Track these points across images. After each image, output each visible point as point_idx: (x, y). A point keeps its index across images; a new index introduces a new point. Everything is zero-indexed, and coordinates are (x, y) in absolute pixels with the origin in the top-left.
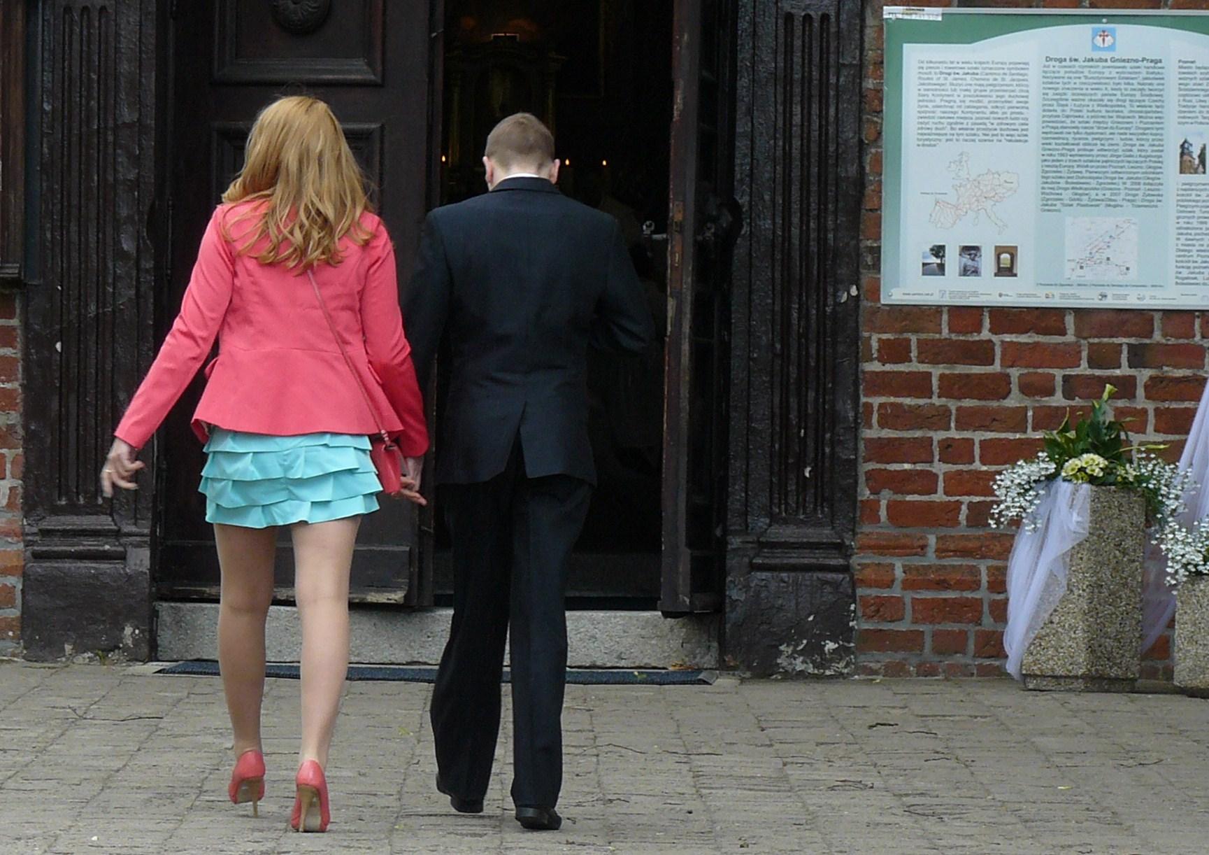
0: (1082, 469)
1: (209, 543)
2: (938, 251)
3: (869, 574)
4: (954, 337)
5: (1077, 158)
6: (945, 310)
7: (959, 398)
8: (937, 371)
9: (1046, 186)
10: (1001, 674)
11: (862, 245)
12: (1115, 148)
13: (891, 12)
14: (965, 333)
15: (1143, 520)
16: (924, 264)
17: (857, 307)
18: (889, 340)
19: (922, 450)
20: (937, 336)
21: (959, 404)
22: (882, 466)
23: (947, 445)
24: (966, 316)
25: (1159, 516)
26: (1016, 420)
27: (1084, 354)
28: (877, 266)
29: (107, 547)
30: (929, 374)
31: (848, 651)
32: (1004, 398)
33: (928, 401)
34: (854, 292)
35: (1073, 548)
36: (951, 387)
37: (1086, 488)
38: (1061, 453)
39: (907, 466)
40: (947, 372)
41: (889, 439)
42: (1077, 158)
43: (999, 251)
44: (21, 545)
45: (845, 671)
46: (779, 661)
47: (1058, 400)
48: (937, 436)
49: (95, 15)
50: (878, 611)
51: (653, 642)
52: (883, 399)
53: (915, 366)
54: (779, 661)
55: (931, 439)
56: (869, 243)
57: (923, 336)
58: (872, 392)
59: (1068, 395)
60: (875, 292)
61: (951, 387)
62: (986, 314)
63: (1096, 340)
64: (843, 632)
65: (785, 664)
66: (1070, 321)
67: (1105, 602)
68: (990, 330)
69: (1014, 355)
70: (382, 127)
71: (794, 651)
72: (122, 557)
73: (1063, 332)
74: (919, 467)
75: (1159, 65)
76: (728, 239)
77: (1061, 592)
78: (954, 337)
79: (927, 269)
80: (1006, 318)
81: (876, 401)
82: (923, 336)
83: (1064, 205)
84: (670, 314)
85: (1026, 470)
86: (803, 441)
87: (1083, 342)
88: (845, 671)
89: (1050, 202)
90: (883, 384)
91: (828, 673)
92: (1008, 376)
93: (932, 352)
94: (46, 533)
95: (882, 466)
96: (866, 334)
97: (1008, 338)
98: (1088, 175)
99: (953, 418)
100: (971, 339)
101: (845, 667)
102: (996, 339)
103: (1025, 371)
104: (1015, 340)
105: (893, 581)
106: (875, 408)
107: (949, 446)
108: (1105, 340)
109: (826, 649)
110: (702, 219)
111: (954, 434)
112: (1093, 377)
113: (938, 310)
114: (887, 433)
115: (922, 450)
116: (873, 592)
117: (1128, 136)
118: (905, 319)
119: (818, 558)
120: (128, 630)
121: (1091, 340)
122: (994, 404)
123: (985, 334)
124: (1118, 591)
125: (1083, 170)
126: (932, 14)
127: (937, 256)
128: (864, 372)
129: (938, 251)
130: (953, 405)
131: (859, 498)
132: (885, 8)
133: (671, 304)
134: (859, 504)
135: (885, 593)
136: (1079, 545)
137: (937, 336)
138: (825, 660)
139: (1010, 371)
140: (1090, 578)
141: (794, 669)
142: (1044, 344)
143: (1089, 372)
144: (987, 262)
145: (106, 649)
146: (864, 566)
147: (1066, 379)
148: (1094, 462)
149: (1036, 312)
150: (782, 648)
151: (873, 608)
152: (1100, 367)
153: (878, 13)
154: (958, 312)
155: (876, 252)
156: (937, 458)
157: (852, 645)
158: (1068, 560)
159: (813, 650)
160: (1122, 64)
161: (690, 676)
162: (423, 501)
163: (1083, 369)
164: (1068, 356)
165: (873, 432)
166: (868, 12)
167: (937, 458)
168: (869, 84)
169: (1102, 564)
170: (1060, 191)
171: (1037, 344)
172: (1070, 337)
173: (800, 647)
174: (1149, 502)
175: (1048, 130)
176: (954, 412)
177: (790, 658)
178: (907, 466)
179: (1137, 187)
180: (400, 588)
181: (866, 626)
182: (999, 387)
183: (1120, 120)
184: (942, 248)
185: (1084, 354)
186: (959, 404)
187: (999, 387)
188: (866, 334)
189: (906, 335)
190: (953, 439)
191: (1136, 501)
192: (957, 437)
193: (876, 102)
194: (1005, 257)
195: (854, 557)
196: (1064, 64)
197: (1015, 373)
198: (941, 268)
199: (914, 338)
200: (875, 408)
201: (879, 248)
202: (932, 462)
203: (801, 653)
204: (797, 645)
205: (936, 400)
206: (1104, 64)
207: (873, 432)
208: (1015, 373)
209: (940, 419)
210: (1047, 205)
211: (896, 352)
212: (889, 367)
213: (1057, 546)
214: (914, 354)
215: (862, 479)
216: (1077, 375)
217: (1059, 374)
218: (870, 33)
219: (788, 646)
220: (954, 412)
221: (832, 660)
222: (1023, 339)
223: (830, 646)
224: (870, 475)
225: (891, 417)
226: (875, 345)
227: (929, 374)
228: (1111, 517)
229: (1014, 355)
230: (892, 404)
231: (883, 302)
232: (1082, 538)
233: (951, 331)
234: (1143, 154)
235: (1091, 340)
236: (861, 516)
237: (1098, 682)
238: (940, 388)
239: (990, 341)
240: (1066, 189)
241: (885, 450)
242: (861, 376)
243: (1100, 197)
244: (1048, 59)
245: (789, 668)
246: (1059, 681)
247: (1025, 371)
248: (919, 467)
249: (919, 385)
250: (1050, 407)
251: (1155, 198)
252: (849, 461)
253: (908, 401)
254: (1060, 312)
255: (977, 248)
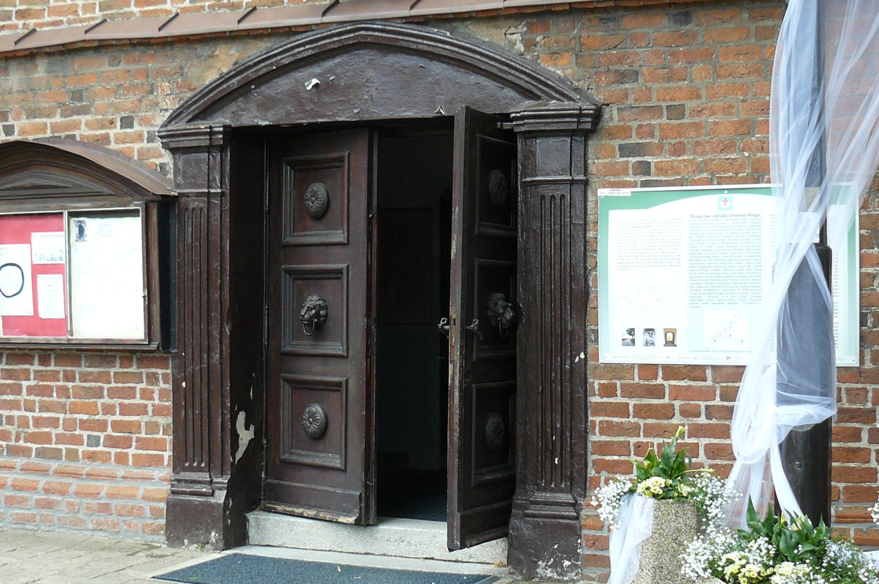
0: (648, 489)
2: (631, 332)
3: (590, 522)
4: (641, 382)
5: (710, 275)
6: (636, 366)
7: (645, 419)
8: (632, 402)
9: (692, 292)
11: (588, 329)
12: (732, 268)
14: (648, 380)
15: (694, 522)
16: (623, 340)
17: (586, 364)
18: (604, 384)
20: (632, 382)
21: (645, 421)
22: (602, 457)
23: (638, 446)
24: (648, 370)
25: (704, 520)
27: (718, 393)
28: (596, 340)
29: (204, 490)
30: (628, 404)
31: (576, 566)
32: (671, 418)
33: (627, 419)
34: (582, 356)
35: (643, 541)
36: (640, 411)
37: (652, 501)
39: (616, 458)
40: (638, 403)
41: (605, 442)
42: (710, 275)
43: (666, 332)
44: (169, 486)
45: (575, 578)
46: (538, 570)
47: (702, 420)
48: (633, 440)
49: (548, 200)
50: (594, 543)
51: (488, 549)
52: (601, 418)
53: (619, 399)
54: (538, 570)
55: (629, 442)
56: (592, 327)
57: (624, 382)
58: (596, 414)
59: (708, 417)
60: (596, 356)
61: (640, 411)
62: (660, 369)
63: (724, 384)
65: (541, 572)
66: (709, 372)
67: (666, 578)
68: (662, 378)
69: (677, 393)
70: (348, 266)
71: (546, 566)
72: (212, 495)
73: (704, 379)
74: (623, 458)
75: (758, 217)
77: (636, 569)
78: (641, 382)
79: (624, 342)
80: (671, 371)
81: (598, 419)
82: (624, 382)
83: (703, 304)
84: (450, 373)
86: (553, 443)
87: (717, 385)
88: (575, 578)
89: (694, 302)
90: (602, 409)
91: (565, 578)
92: (673, 405)
93: (630, 391)
94: (179, 481)
95: (602, 457)
96: (591, 380)
97: (673, 383)
98: (717, 285)
99: (642, 429)
100: (651, 383)
101: (575, 576)
102: (666, 383)
103: (683, 402)
104: (677, 384)
105: (603, 527)
106: (597, 424)
107: (639, 446)
108: (730, 384)
109: (564, 565)
111: (642, 439)
112: (723, 406)
113: (632, 366)
114: (604, 438)
116: (592, 532)
117: (740, 261)
118: (613, 372)
119: (560, 512)
120: (213, 534)
121: (722, 384)
122: (665, 422)
123: (660, 381)
124: (675, 570)
125: (714, 282)
127: (630, 334)
128: (590, 402)
129: (631, 332)
130: (642, 422)
131: (589, 476)
132: (599, 190)
133: (451, 366)
134: (588, 479)
135: (598, 533)
136: (647, 539)
137: (632, 382)
138: (564, 571)
139: (674, 402)
140: (653, 563)
141: (546, 576)
142: (694, 386)
143: (721, 403)
144: (659, 338)
146: (588, 516)
147: (707, 407)
148: (657, 483)
149: (689, 367)
150: (540, 563)
151: (591, 542)
152: (727, 401)
153: (595, 194)
154: (643, 367)
155: (596, 332)
156: (632, 453)
157: (579, 563)
158: (640, 548)
160: (737, 218)
163: (718, 402)
164: (708, 394)
166: (590, 193)
167: (632, 453)
168: (590, 234)
169: (663, 553)
170: (700, 295)
171: (689, 386)
172: (709, 383)
173: (550, 563)
174: (698, 510)
175: (693, 258)
176: (642, 426)
178: (616, 458)
179: (746, 292)
180: (354, 513)
181: (587, 552)
182: (667, 412)
183: (735, 251)
184: (633, 330)
185: (718, 393)
186: (645, 421)
187: (667, 412)
188: (591, 380)
189: (614, 381)
190: (642, 442)
191: (689, 510)
192: (644, 441)
193: (595, 245)
194: (670, 336)
195: (583, 511)
196: (701, 219)
197: (677, 404)
198: (633, 341)
199: (618, 383)
200: (597, 424)
201: (598, 330)
202: (629, 455)
203: (550, 567)
204: (548, 562)
205: (631, 419)
206: (725, 218)
208: (677, 404)
209: (634, 430)
212: (605, 400)
214: (619, 392)
215: (590, 465)
216: (714, 405)
217: (703, 404)
218: (590, 205)
219: (543, 561)
220: (642, 426)
221: (567, 572)
222: (681, 383)
223: (567, 563)
224: (595, 462)
225: (607, 429)
226: (597, 387)
227: (628, 404)
228: (670, 521)
229: (677, 393)
230: (607, 421)
231: (600, 361)
232: (649, 536)
233: (640, 378)
234: (750, 272)
235: (722, 384)
236: (590, 486)
238: (634, 412)
239: (662, 385)
240: (704, 294)
241: (603, 448)
242: (589, 405)
243: (725, 298)
244: (692, 216)
245: (544, 575)
247: (683, 402)
248: (623, 458)
249: (622, 410)
250: (697, 424)
251: (757, 298)
252: (581, 455)
253: (616, 420)
254: (703, 368)
255: (653, 330)
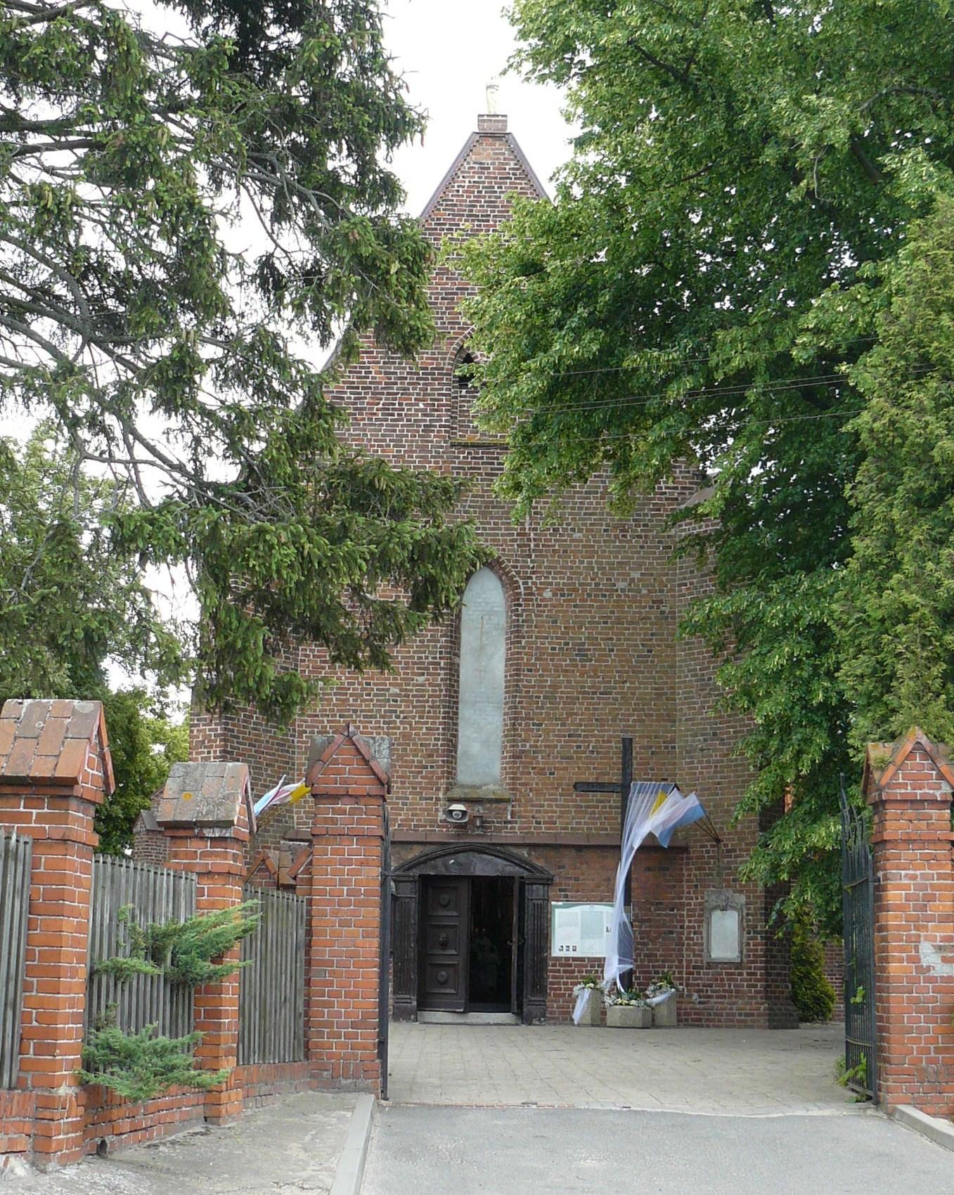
1: (456, 989)
10: (573, 1025)
13: (553, 903)
19: (559, 983)
24: (567, 959)
26: (577, 978)
36: (565, 972)
38: (585, 984)
53: (558, 968)
64: (544, 1016)
76: (524, 944)
80: (575, 959)
85: (579, 986)
90: (552, 971)
110: (519, 940)
115: (559, 983)
126: (561, 903)
144: (571, 949)
145: (408, 1019)
148: (592, 985)
159: (540, 1020)
161: (517, 1025)
162: (879, 1064)
165: (550, 980)
177: (535, 1021)
207: (550, 980)
210: (582, 938)
211: (554, 965)
213: (585, 1000)
225: (554, 977)
237: (593, 1025)
241: (552, 983)
246: (585, 1025)
249: (559, 971)
